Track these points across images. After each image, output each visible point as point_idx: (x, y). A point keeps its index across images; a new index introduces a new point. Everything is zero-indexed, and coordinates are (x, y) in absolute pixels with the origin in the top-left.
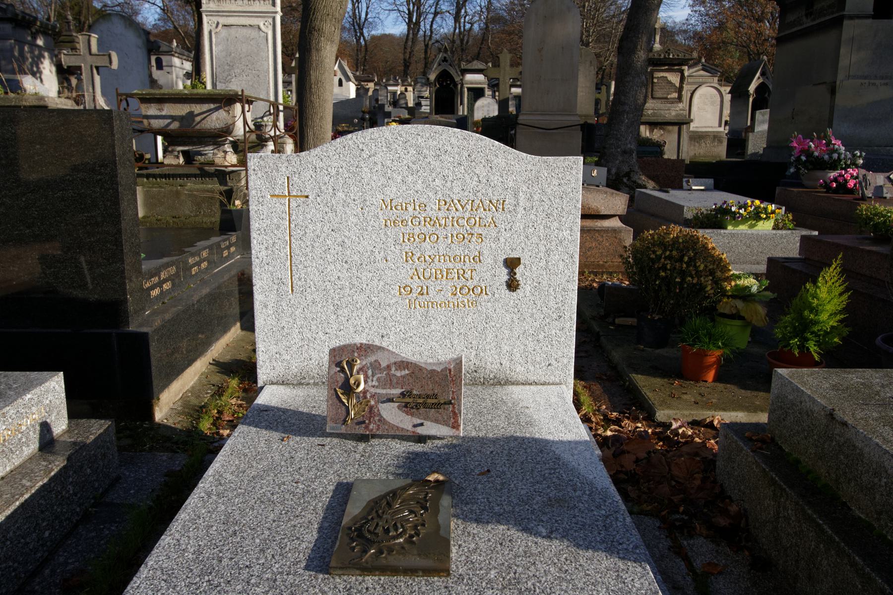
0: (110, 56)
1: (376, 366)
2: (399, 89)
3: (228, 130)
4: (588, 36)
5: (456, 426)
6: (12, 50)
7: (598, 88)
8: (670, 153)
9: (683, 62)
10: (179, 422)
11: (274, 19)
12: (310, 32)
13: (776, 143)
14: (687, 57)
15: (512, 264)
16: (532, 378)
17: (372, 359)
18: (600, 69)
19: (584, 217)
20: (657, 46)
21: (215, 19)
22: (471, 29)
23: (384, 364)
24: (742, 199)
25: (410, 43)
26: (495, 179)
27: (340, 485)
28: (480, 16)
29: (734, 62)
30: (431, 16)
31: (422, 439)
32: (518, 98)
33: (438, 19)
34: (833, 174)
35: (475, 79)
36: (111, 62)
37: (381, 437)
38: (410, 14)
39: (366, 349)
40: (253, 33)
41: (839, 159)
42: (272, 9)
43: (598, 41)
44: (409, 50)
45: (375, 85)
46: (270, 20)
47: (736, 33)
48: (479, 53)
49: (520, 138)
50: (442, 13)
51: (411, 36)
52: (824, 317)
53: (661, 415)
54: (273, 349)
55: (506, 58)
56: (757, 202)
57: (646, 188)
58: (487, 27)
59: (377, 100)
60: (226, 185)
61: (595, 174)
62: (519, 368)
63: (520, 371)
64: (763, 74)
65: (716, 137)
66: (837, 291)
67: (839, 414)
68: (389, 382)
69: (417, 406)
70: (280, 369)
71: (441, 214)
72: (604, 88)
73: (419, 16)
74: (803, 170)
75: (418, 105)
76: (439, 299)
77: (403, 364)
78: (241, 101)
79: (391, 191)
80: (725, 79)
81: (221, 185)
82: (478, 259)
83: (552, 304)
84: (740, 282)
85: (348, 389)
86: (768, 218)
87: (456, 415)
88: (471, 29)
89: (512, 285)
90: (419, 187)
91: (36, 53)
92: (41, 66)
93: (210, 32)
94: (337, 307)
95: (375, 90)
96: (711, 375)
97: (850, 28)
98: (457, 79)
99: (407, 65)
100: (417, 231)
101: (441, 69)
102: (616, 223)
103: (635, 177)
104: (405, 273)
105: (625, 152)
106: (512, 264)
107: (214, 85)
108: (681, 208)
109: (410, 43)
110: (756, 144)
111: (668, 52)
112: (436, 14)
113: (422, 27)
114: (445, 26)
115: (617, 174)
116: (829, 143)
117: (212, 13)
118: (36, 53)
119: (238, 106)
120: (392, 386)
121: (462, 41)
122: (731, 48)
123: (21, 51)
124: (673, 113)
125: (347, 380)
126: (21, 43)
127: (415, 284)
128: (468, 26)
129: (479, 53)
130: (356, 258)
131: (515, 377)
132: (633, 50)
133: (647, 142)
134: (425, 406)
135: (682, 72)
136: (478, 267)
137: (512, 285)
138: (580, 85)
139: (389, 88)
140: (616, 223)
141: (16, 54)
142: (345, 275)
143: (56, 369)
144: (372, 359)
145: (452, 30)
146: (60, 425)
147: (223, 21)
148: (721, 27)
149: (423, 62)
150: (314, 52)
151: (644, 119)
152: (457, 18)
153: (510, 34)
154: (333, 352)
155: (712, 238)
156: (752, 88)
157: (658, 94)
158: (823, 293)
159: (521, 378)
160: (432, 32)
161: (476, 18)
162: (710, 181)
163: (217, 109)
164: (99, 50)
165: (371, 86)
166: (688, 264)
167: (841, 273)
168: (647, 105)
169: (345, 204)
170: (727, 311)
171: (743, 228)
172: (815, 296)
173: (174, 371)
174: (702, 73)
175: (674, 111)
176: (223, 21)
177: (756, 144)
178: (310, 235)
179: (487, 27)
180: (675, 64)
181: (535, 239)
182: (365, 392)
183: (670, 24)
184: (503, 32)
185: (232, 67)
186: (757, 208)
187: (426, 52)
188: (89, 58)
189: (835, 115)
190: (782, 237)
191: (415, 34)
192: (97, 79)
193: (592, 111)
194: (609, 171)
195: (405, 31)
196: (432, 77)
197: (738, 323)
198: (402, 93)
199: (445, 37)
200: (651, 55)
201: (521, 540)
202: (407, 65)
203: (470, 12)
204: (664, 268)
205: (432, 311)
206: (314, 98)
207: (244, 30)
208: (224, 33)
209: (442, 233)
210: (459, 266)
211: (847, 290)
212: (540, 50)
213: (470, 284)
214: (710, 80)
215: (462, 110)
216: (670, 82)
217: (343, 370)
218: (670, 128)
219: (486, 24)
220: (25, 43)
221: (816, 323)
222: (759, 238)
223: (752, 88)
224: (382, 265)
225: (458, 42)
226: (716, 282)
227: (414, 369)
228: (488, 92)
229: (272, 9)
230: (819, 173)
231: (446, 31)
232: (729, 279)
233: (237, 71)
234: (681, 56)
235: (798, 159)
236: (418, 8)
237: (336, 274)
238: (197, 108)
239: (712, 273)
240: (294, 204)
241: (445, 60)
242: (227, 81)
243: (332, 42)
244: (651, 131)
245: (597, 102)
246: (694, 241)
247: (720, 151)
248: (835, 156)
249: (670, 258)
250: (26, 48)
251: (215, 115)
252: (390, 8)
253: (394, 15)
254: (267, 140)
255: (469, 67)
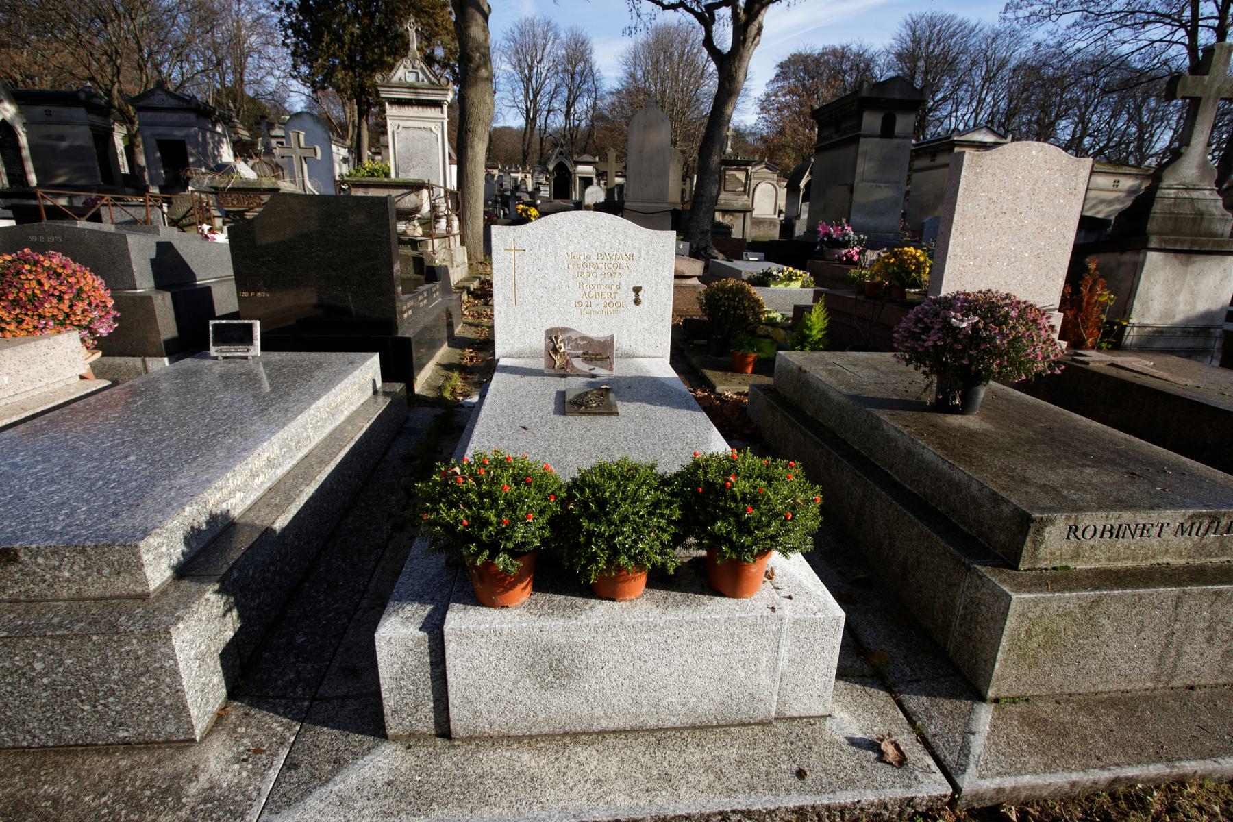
0: (315, 149)
1: (569, 339)
2: (520, 176)
3: (417, 210)
4: (676, 136)
5: (611, 369)
6: (196, 136)
7: (684, 180)
8: (736, 234)
9: (749, 163)
10: (430, 394)
11: (442, 123)
12: (466, 133)
13: (811, 230)
14: (751, 159)
15: (637, 290)
16: (647, 354)
17: (567, 335)
18: (685, 164)
19: (677, 277)
20: (729, 150)
21: (397, 122)
22: (579, 125)
23: (574, 338)
24: (781, 267)
25: (528, 135)
26: (629, 242)
27: (558, 392)
28: (587, 114)
29: (790, 162)
30: (545, 113)
31: (594, 376)
32: (621, 186)
33: (551, 115)
34: (844, 251)
35: (585, 170)
36: (316, 154)
37: (572, 376)
38: (528, 111)
39: (564, 330)
40: (427, 134)
41: (849, 240)
42: (441, 116)
43: (683, 140)
44: (527, 142)
45: (500, 171)
46: (440, 125)
47: (793, 138)
48: (586, 147)
49: (1083, 233)
50: (554, 110)
51: (529, 130)
52: (814, 332)
53: (719, 389)
54: (504, 337)
55: (612, 155)
56: (791, 269)
57: (717, 258)
58: (593, 125)
59: (502, 185)
60: (417, 250)
61: (681, 246)
62: (640, 349)
63: (640, 350)
64: (810, 173)
65: (771, 222)
66: (822, 318)
67: (804, 368)
68: (577, 347)
69: (591, 360)
70: (508, 349)
71: (599, 261)
72: (688, 180)
73: (536, 111)
74: (825, 248)
75: (537, 190)
76: (597, 309)
77: (584, 338)
78: (427, 188)
79: (572, 248)
80: (783, 174)
81: (413, 249)
82: (619, 287)
83: (659, 312)
84: (771, 315)
85: (556, 351)
86: (797, 280)
87: (611, 364)
88: (579, 125)
89: (637, 302)
90: (587, 246)
91: (217, 139)
92: (221, 150)
93: (393, 133)
94: (541, 313)
95: (500, 176)
96: (750, 369)
97: (865, 145)
98: (571, 170)
99: (525, 155)
100: (585, 271)
101: (558, 161)
102: (695, 281)
103: (710, 251)
104: (578, 294)
105: (703, 232)
106: (637, 290)
107: (397, 174)
108: (740, 272)
109: (528, 135)
110: (800, 229)
111: (737, 155)
112: (549, 111)
113: (538, 123)
114: (557, 122)
115: (697, 248)
116: (843, 229)
117: (394, 117)
118: (217, 139)
119: (425, 192)
120: (578, 349)
121: (572, 135)
122: (789, 150)
123: (204, 137)
124: (740, 203)
125: (555, 346)
126: (204, 130)
127: (584, 301)
128: (577, 123)
129: (586, 147)
130: (551, 285)
131: (638, 353)
132: (709, 156)
133: (720, 225)
134: (596, 359)
135: (747, 171)
136: (618, 291)
137: (637, 302)
138: (670, 178)
139: (512, 175)
140: (695, 281)
141: (200, 139)
142: (545, 295)
143: (376, 351)
144: (567, 335)
145: (563, 125)
146: (379, 384)
147: (403, 123)
148: (781, 132)
149: (539, 152)
150: (469, 149)
151: (717, 207)
152: (567, 115)
153: (611, 130)
154: (547, 331)
155: (757, 291)
156: (802, 184)
157: (729, 188)
158: (814, 318)
159: (642, 354)
160: (546, 127)
161: (584, 116)
162: (762, 255)
163: (409, 193)
164: (305, 144)
165: (496, 172)
166: (739, 302)
167: (825, 306)
168: (721, 196)
169: (546, 255)
170: (762, 333)
171: (781, 286)
172: (810, 320)
173: (422, 366)
174: (765, 170)
175: (741, 201)
176: (403, 123)
177: (800, 229)
178: (526, 272)
179: (593, 125)
180: (742, 165)
181: (650, 276)
182: (564, 352)
183: (742, 127)
184: (606, 128)
185: (410, 160)
186: (790, 273)
187: (541, 144)
188: (298, 150)
189: (853, 209)
190: (806, 292)
191: (533, 128)
192: (305, 166)
193: (679, 200)
194: (691, 246)
195: (524, 126)
196: (551, 167)
197: (768, 341)
198: (522, 180)
199: (557, 131)
200: (723, 157)
201: (648, 407)
202: (525, 155)
203: (578, 111)
204: (724, 306)
205: (593, 316)
206: (470, 185)
207: (420, 132)
208: (404, 133)
209: (599, 272)
210: (608, 291)
211: (828, 316)
212: (641, 152)
213: (615, 301)
214: (771, 176)
215: (575, 196)
216: (738, 179)
217: (552, 341)
218: (737, 214)
219: (592, 121)
220: (208, 130)
221: (810, 336)
222: (791, 293)
223: (802, 184)
224: (567, 289)
225: (569, 136)
226: (756, 314)
227: (589, 341)
228: (595, 181)
229: (441, 116)
230: (836, 250)
231: (558, 126)
232: (763, 313)
233: (415, 163)
234: (746, 158)
235: (822, 239)
236: (535, 106)
237: (540, 294)
238: (395, 193)
239: (753, 308)
240: (517, 255)
241: (561, 153)
242: (408, 171)
243: (483, 141)
244: (724, 217)
245: (683, 191)
246: (743, 288)
247: (775, 234)
248: (847, 238)
249: (727, 298)
250: (208, 135)
251: (407, 198)
252: (511, 104)
253: (515, 110)
254: (440, 217)
255: (580, 159)
